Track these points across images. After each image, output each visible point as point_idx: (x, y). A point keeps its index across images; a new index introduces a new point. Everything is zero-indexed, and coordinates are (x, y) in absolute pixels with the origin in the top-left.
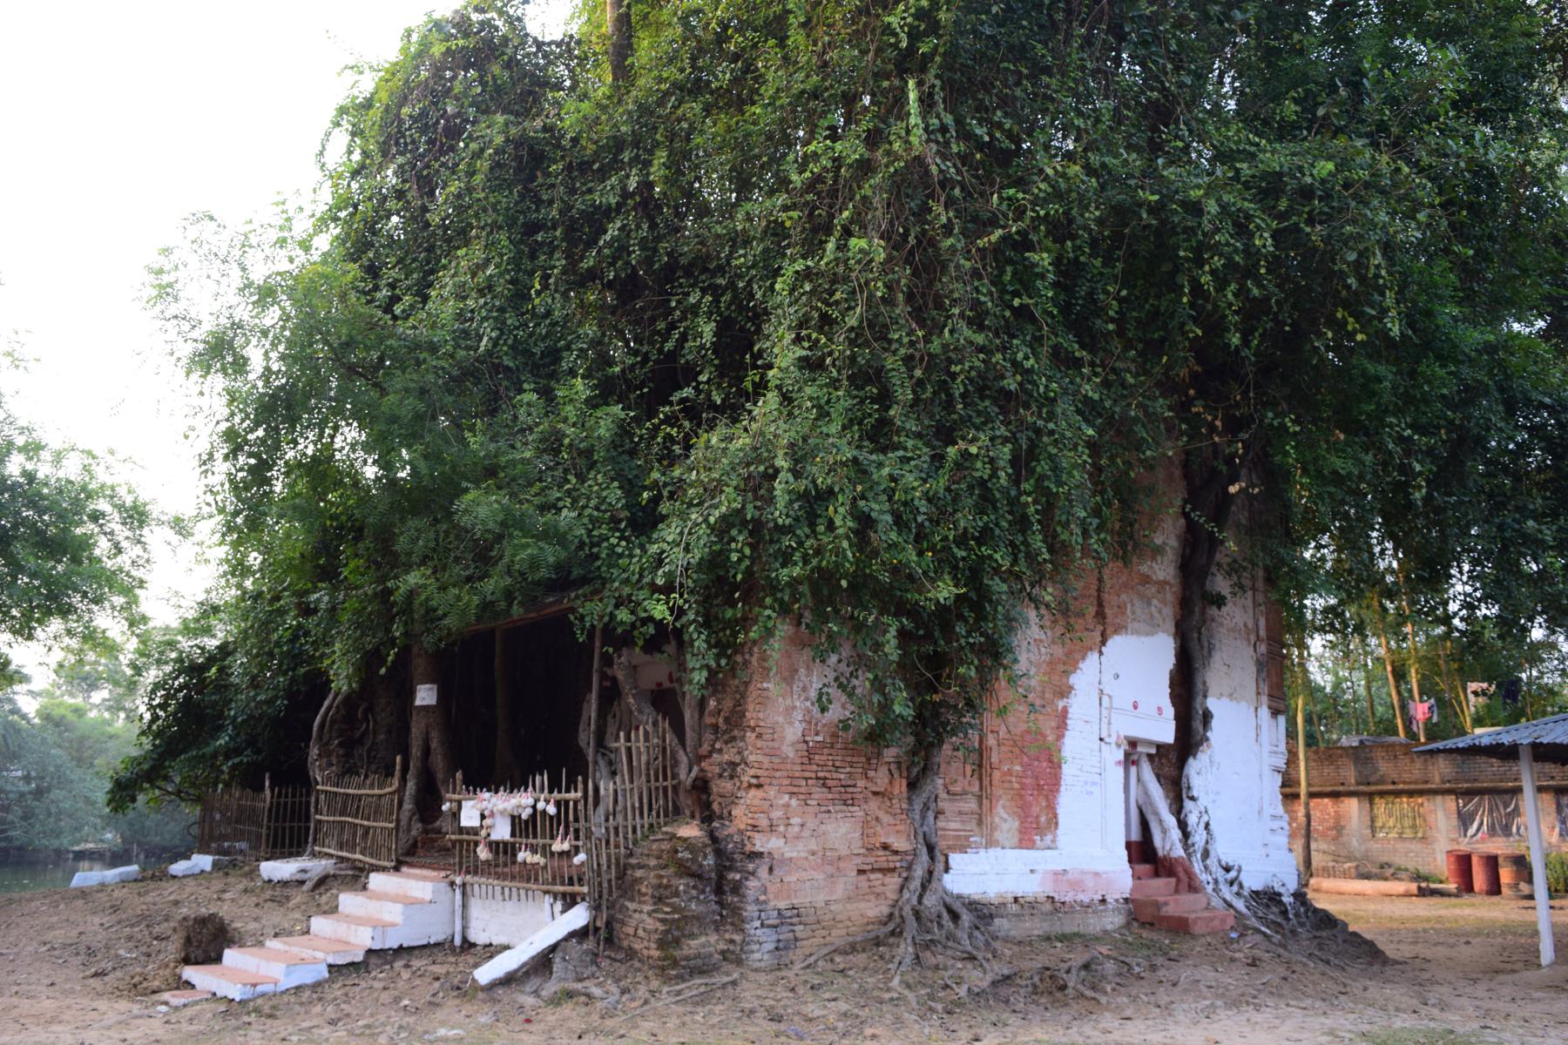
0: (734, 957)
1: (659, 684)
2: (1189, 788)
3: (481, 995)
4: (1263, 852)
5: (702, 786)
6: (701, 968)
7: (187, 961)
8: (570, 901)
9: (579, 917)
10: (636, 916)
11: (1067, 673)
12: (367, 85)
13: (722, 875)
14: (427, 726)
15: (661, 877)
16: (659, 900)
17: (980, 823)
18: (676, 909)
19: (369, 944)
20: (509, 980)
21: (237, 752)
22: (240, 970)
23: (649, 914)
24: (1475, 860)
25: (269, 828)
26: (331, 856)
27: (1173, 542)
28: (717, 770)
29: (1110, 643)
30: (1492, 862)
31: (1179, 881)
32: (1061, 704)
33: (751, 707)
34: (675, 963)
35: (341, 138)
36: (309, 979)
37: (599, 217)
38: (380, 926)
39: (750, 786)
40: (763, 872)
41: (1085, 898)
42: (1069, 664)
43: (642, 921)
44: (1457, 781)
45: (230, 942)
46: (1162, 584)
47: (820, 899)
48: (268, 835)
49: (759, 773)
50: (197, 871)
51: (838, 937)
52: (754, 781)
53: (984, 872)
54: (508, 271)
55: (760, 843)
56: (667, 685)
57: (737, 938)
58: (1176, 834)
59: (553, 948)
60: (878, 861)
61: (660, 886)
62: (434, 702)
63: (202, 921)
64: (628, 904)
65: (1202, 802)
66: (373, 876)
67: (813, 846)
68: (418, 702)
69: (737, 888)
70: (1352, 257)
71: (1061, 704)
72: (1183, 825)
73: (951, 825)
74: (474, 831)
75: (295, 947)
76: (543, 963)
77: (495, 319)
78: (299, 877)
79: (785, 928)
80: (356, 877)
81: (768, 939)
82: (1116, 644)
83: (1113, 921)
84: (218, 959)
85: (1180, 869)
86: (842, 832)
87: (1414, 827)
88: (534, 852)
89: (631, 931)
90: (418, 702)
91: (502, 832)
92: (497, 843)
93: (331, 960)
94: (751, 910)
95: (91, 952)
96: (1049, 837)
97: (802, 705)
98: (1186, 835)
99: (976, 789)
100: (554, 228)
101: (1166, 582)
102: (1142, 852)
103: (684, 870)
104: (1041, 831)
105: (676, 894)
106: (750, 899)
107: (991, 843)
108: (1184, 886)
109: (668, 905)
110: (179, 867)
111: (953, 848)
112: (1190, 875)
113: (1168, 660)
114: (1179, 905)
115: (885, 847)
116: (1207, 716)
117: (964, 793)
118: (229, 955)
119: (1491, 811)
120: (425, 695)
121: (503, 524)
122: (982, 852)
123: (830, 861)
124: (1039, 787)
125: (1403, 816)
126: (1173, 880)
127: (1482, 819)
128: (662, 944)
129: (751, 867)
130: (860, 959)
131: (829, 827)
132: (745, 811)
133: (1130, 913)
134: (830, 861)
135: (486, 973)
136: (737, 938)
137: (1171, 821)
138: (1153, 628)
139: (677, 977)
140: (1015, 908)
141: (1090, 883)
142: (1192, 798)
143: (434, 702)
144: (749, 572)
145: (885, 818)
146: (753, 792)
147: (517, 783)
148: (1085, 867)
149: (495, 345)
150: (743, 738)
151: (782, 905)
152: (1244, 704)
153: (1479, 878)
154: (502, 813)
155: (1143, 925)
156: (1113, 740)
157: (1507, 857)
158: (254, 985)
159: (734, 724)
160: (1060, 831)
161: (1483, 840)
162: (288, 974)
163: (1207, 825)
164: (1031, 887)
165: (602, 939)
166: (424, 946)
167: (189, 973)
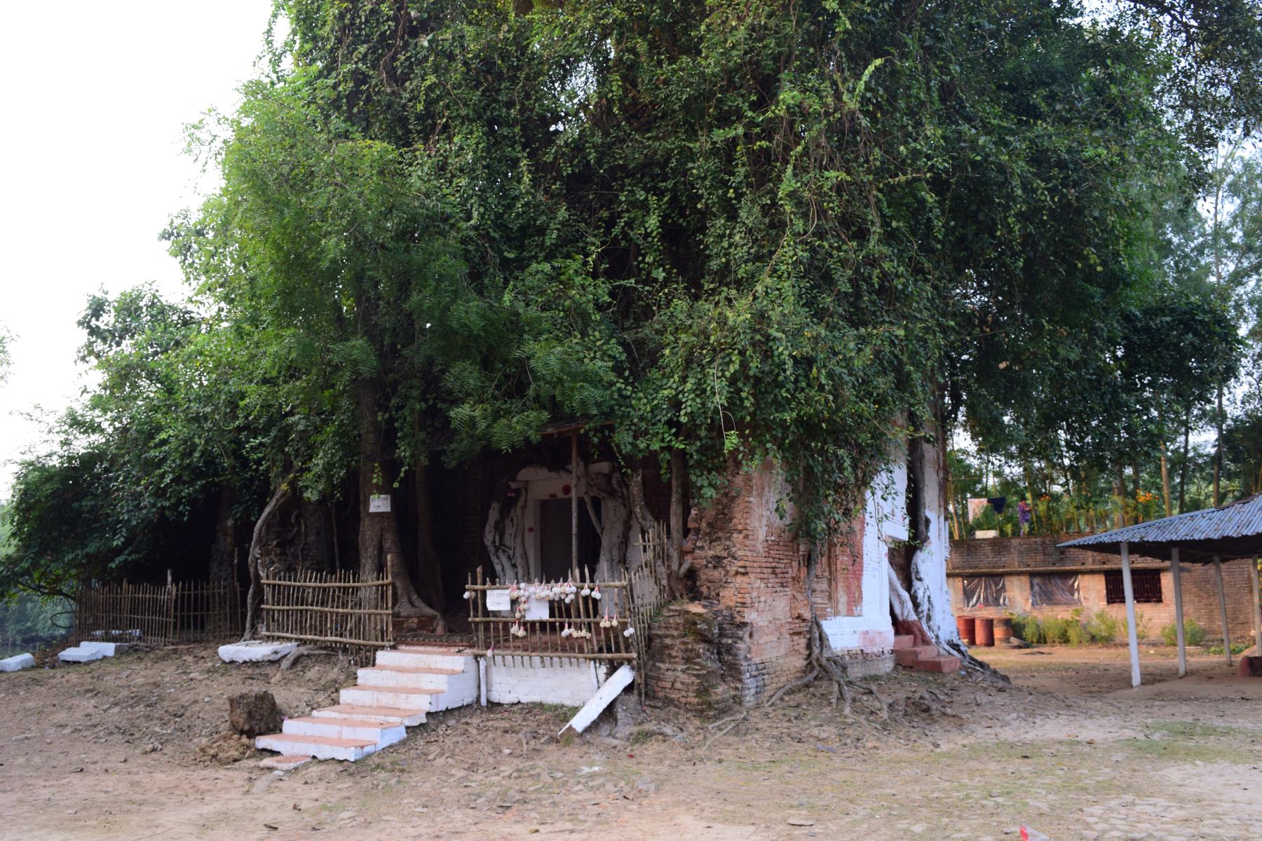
0: (738, 700)
1: (553, 496)
2: (917, 572)
3: (577, 740)
6: (723, 711)
8: (613, 668)
9: (624, 676)
10: (670, 673)
13: (721, 642)
14: (382, 529)
15: (685, 643)
17: (830, 598)
19: (428, 708)
20: (594, 726)
23: (683, 671)
24: (978, 623)
25: (175, 617)
26: (289, 639)
28: (704, 562)
30: (989, 624)
31: (915, 637)
33: (738, 516)
34: (710, 706)
36: (395, 740)
39: (737, 573)
44: (963, 568)
48: (175, 624)
49: (747, 564)
50: (100, 656)
52: (742, 570)
54: (484, 158)
56: (561, 495)
57: (739, 686)
58: (910, 605)
61: (686, 650)
62: (389, 510)
64: (661, 665)
65: (926, 581)
66: (379, 654)
68: (372, 509)
72: (914, 599)
76: (609, 713)
77: (479, 196)
78: (273, 657)
79: (760, 678)
83: (887, 666)
85: (916, 629)
88: (579, 628)
89: (668, 685)
90: (372, 509)
91: (540, 613)
92: (533, 623)
93: (408, 724)
98: (916, 605)
99: (827, 574)
100: (513, 126)
105: (699, 656)
106: (741, 657)
107: (836, 613)
108: (919, 640)
109: (696, 664)
110: (70, 653)
112: (921, 631)
114: (926, 654)
118: (288, 726)
119: (986, 589)
126: (912, 637)
127: (981, 593)
128: (699, 693)
129: (741, 633)
130: (799, 697)
135: (579, 722)
136: (739, 686)
139: (715, 716)
142: (920, 580)
143: (389, 510)
146: (739, 579)
149: (483, 217)
150: (729, 539)
153: (980, 635)
154: (540, 600)
155: (905, 668)
157: (1000, 621)
158: (362, 747)
161: (980, 609)
162: (382, 736)
166: (459, 708)
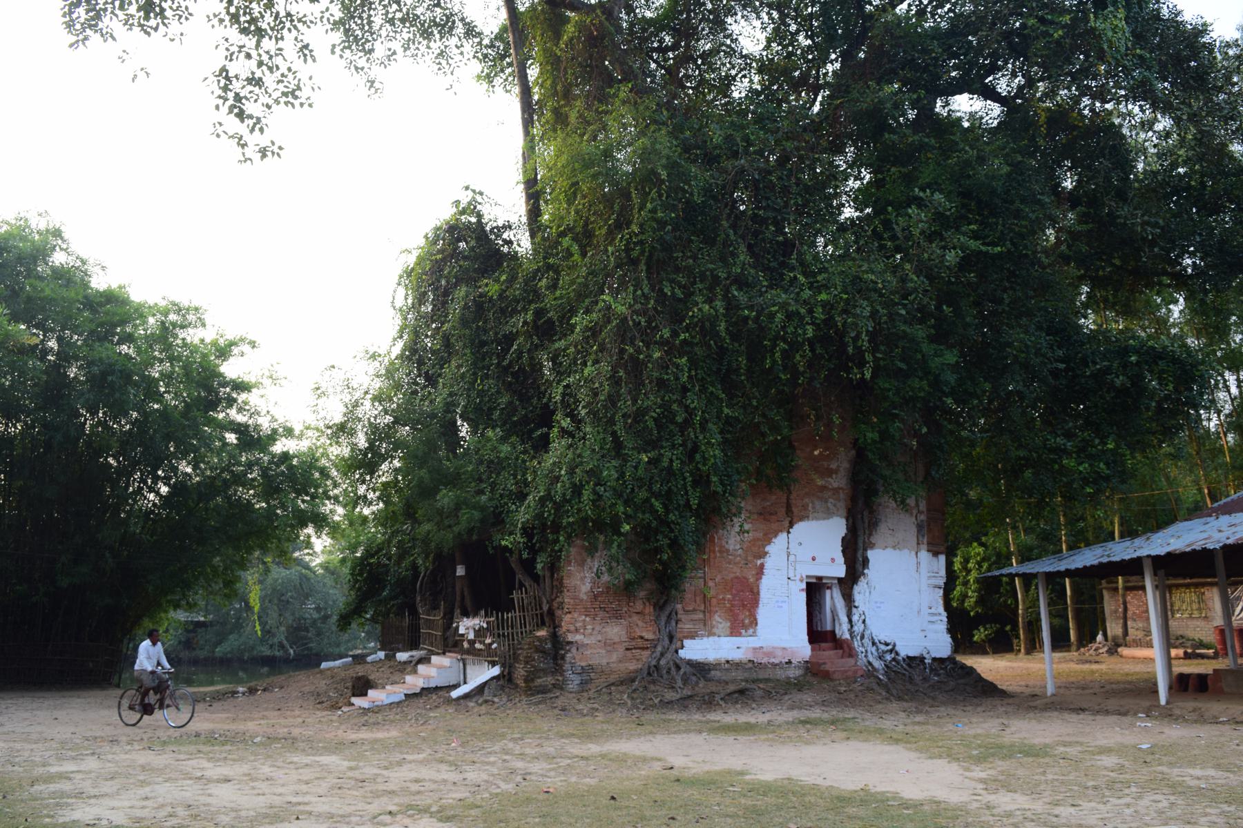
4: (923, 634)
5: (551, 613)
6: (543, 690)
7: (354, 695)
8: (493, 664)
9: (496, 671)
11: (764, 546)
12: (412, 260)
13: (557, 649)
16: (527, 663)
18: (533, 666)
20: (466, 696)
21: (395, 598)
22: (376, 696)
27: (846, 465)
29: (796, 527)
32: (759, 562)
35: (401, 292)
36: (397, 700)
37: (509, 339)
38: (428, 678)
40: (574, 650)
41: (776, 661)
42: (768, 538)
43: (520, 672)
45: (372, 687)
46: (836, 490)
47: (604, 662)
51: (613, 678)
53: (708, 647)
55: (570, 638)
58: (846, 626)
59: (486, 683)
60: (635, 644)
63: (359, 679)
65: (861, 609)
67: (599, 638)
69: (563, 658)
70: (853, 335)
71: (759, 562)
72: (850, 621)
73: (686, 626)
74: (463, 635)
75: (396, 688)
76: (480, 689)
80: (425, 660)
81: (576, 680)
82: (800, 528)
84: (366, 695)
86: (615, 631)
87: (1199, 609)
94: (567, 666)
95: (318, 695)
96: (751, 631)
97: (589, 576)
101: (840, 488)
102: (816, 635)
103: (537, 650)
104: (746, 628)
107: (711, 634)
111: (687, 638)
113: (842, 531)
115: (642, 638)
116: (866, 562)
117: (694, 610)
120: (460, 571)
121: (457, 504)
122: (705, 639)
123: (609, 645)
124: (744, 606)
125: (1192, 602)
128: (526, 681)
131: (608, 629)
132: (566, 622)
133: (807, 668)
134: (609, 645)
137: (844, 619)
138: (828, 514)
140: (750, 665)
141: (779, 653)
144: (553, 521)
145: (640, 623)
147: (475, 615)
148: (776, 645)
151: (583, 664)
152: (906, 551)
156: (798, 577)
159: (559, 587)
160: (759, 627)
163: (864, 621)
164: (737, 656)
165: (505, 681)
167: (354, 700)
